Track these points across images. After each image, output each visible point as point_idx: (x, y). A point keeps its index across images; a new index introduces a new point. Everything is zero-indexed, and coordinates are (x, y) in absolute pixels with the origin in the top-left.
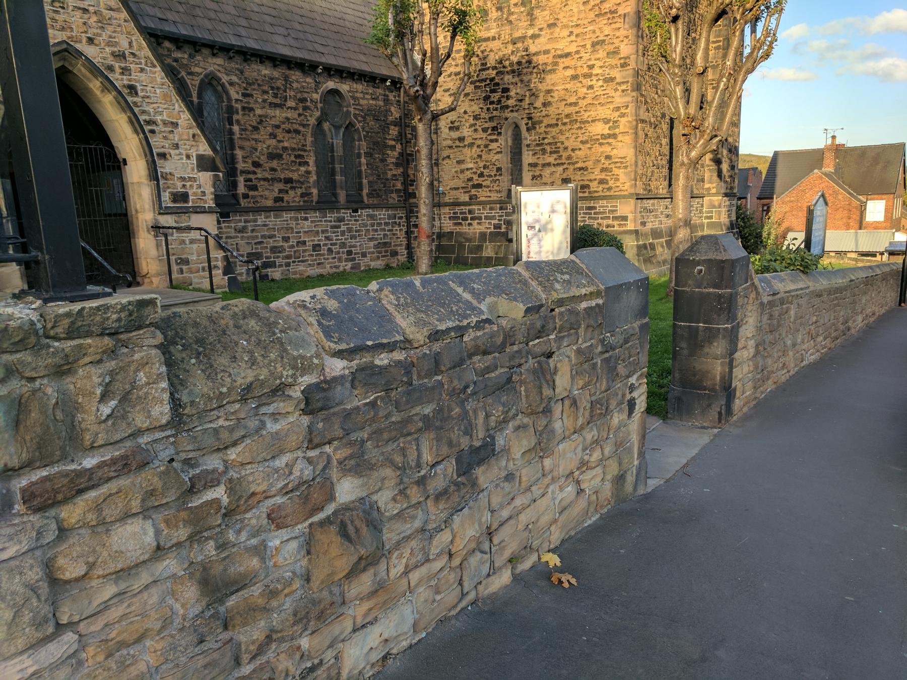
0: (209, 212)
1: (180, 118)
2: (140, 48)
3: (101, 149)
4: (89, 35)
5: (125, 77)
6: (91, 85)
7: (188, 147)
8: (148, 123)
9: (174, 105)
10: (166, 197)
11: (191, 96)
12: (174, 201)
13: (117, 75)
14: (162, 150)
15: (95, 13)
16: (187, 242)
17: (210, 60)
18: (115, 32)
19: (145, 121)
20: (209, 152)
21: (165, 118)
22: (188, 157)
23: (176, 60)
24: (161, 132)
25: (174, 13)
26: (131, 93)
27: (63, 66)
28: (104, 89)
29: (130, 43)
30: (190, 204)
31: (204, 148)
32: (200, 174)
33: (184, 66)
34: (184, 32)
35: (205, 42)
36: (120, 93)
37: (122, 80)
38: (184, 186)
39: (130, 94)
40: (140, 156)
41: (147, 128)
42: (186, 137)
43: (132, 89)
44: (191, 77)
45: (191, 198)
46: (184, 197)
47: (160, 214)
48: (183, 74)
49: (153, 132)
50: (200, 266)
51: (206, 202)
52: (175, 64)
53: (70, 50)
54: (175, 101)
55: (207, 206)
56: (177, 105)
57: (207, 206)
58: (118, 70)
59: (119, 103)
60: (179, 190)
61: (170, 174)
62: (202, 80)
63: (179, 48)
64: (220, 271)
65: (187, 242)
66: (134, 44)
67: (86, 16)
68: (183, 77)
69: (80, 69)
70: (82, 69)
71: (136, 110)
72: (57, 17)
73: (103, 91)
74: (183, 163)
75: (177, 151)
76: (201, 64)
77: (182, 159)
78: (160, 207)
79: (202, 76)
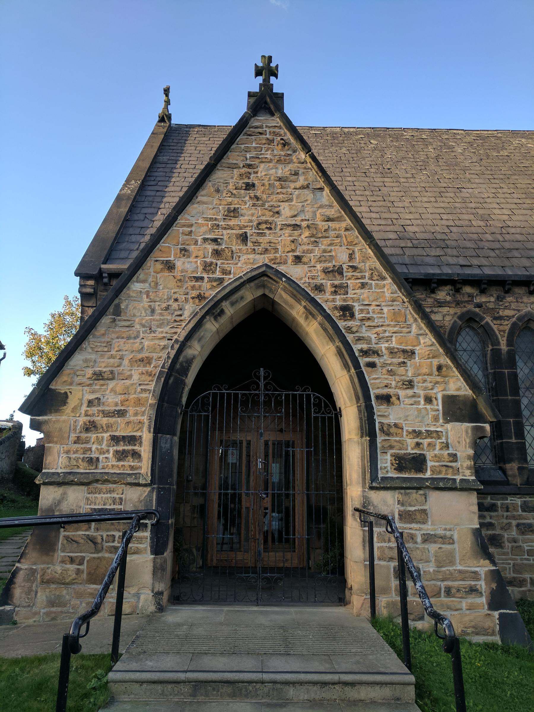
0: (462, 490)
1: (420, 344)
2: (365, 259)
3: (308, 396)
4: (298, 254)
5: (338, 297)
6: (294, 313)
7: (430, 385)
8: (365, 353)
9: (409, 326)
10: (386, 462)
11: (499, 344)
12: (400, 468)
13: (328, 296)
14: (385, 391)
15: (308, 227)
16: (419, 539)
17: (525, 300)
18: (331, 245)
19: (361, 351)
20: (466, 391)
21: (394, 344)
22: (429, 400)
23: (479, 306)
24: (384, 365)
25: (482, 259)
26: (344, 315)
27: (264, 295)
28: (309, 314)
29: (351, 256)
30: (428, 474)
31: (457, 386)
32: (449, 426)
33: (489, 311)
34: (488, 271)
35: (517, 279)
36: (328, 317)
37: (334, 300)
38: (418, 445)
39: (343, 317)
40: (350, 400)
41: (363, 361)
42: (425, 370)
43: (347, 311)
44: (498, 322)
45: (430, 464)
46: (418, 462)
47: (372, 488)
48: (488, 319)
49: (372, 365)
50: (443, 585)
51: (457, 471)
52: (477, 310)
53: (270, 272)
54: (411, 320)
55: (458, 478)
56: (414, 326)
57: (458, 478)
58: (329, 289)
59: (325, 330)
60: (410, 451)
61: (396, 425)
62: (514, 325)
63: (483, 292)
64: (483, 600)
65: (419, 539)
66: (357, 255)
67: (296, 233)
68: (487, 323)
69: (282, 296)
70: (283, 293)
71: (350, 338)
72: (261, 239)
73: (307, 318)
74: (419, 410)
75: (410, 392)
76: (513, 306)
77: (418, 403)
78: (374, 477)
79: (514, 319)
